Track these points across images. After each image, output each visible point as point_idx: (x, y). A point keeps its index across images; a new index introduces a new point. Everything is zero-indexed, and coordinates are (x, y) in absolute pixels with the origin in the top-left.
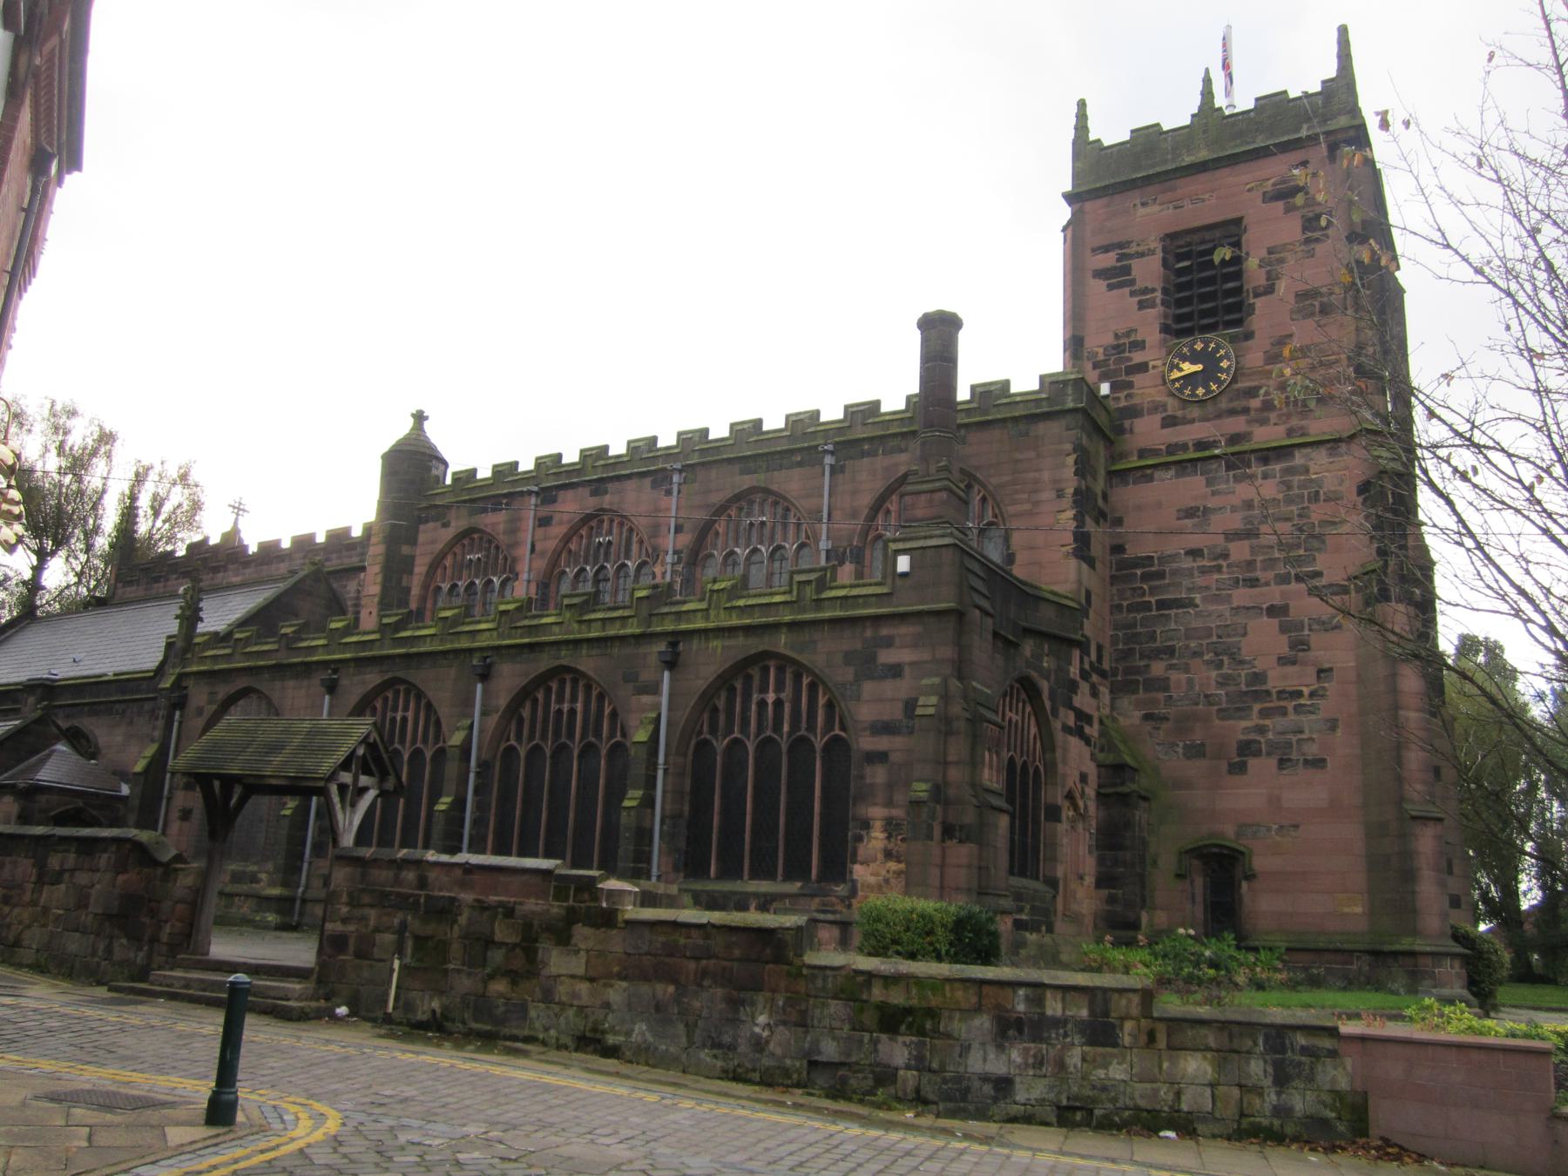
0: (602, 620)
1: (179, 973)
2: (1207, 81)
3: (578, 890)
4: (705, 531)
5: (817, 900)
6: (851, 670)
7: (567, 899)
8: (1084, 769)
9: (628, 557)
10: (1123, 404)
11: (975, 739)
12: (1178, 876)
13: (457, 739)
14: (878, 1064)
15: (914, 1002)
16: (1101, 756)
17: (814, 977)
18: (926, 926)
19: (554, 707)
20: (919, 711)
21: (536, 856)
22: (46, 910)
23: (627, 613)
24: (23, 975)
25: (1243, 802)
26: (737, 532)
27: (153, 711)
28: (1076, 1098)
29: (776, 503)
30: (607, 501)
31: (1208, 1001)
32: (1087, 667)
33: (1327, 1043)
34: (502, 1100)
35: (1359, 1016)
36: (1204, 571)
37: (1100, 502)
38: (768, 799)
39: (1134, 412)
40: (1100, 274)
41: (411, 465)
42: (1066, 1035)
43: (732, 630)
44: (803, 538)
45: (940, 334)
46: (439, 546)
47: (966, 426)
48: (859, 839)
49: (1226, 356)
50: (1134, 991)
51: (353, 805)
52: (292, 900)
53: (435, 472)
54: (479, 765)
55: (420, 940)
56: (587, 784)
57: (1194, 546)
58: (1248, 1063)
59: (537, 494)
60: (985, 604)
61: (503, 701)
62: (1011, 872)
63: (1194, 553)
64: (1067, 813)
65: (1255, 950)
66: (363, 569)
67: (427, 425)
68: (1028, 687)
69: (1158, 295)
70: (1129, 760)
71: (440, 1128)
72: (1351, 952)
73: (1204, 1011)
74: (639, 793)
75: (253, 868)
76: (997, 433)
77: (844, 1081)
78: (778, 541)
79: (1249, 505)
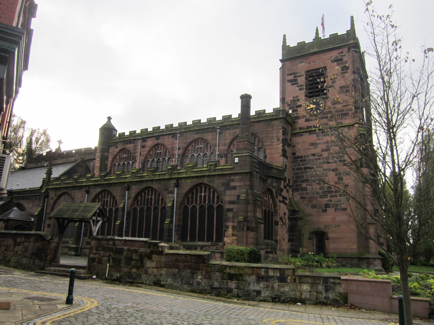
0: (159, 174)
1: (52, 268)
2: (317, 30)
3: (154, 246)
4: (186, 149)
5: (215, 247)
6: (223, 187)
7: (151, 248)
8: (285, 212)
9: (166, 156)
10: (295, 115)
11: (255, 206)
12: (310, 239)
13: (121, 206)
14: (228, 288)
15: (237, 272)
16: (289, 208)
17: (212, 267)
18: (242, 253)
19: (147, 197)
20: (241, 198)
21: (142, 237)
22: (17, 252)
23: (165, 173)
24: (11, 269)
25: (326, 219)
26: (194, 149)
27: (40, 198)
28: (277, 295)
29: (204, 142)
30: (160, 141)
31: (309, 271)
32: (285, 185)
33: (338, 281)
34: (136, 298)
35: (348, 274)
36: (316, 159)
37: (289, 141)
38: (202, 219)
39: (298, 118)
40: (289, 81)
41: (107, 131)
42: (274, 280)
43: (193, 177)
44: (212, 151)
45: (246, 100)
46: (115, 153)
47: (254, 122)
48: (226, 231)
49: (322, 103)
50: (291, 269)
51: (96, 225)
52: (78, 248)
53: (114, 133)
54: (127, 212)
55: (114, 259)
56: (156, 218)
57: (314, 153)
58: (318, 286)
59: (141, 139)
60: (258, 170)
61: (133, 196)
62: (265, 238)
63: (314, 155)
64: (280, 223)
65: (329, 258)
66: (95, 159)
67: (111, 120)
68: (269, 191)
69: (304, 87)
70: (296, 209)
71: (121, 304)
72: (353, 258)
73: (307, 274)
74: (169, 220)
75: (68, 240)
76: (262, 124)
77: (220, 292)
78: (205, 152)
79: (327, 142)
